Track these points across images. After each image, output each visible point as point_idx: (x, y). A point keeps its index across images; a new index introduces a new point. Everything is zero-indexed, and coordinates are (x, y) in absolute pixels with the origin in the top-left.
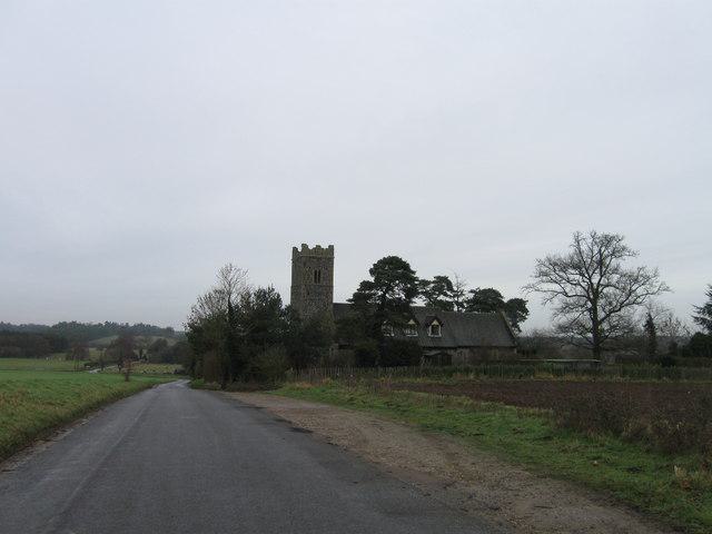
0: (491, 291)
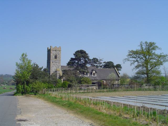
0: (111, 62)
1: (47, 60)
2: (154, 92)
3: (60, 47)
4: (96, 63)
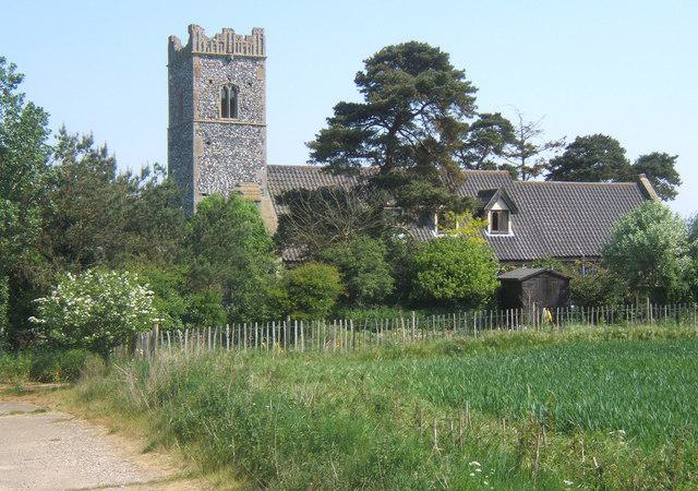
2: (268, 64)
3: (259, 34)
4: (498, 152)
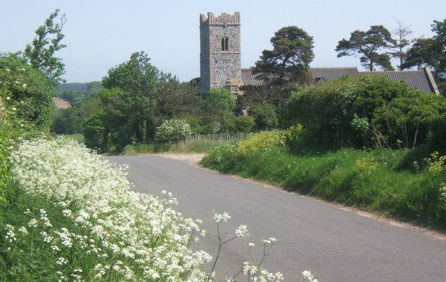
1: (201, 55)
2: (241, 27)
3: (237, 15)
